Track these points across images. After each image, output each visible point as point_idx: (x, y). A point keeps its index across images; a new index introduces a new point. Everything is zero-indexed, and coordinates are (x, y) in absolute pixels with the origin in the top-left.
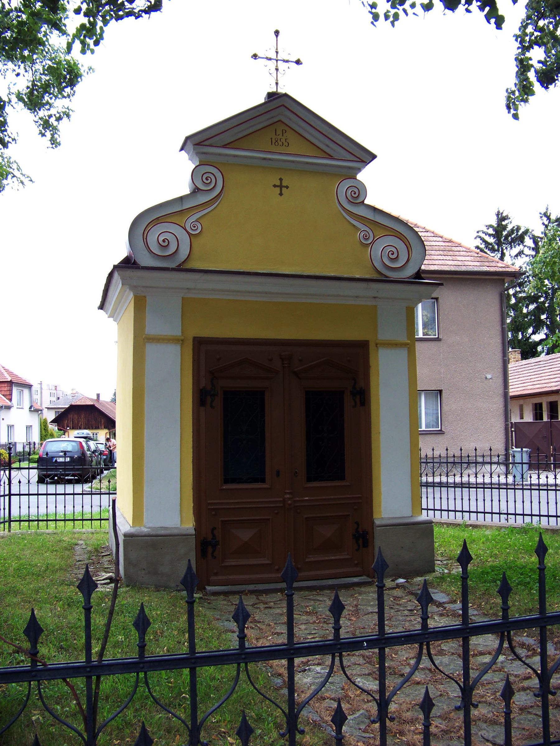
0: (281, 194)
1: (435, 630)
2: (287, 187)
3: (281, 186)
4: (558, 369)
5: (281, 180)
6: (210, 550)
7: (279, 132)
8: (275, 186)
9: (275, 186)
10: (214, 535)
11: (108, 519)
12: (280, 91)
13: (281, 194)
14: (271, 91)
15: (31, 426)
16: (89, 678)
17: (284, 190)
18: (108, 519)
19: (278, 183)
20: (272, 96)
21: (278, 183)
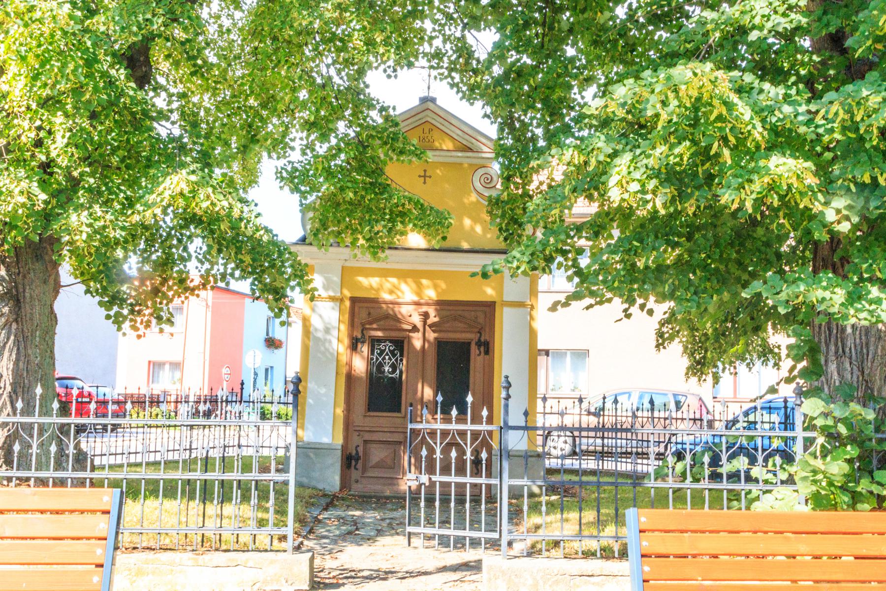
0: (425, 183)
1: (609, 465)
2: (430, 177)
3: (425, 176)
4: (12, 525)
5: (425, 171)
6: (353, 463)
7: (426, 130)
8: (420, 176)
9: (420, 176)
10: (357, 451)
11: (108, 512)
12: (431, 95)
13: (425, 183)
14: (422, 96)
15: (272, 367)
16: (603, 426)
17: (427, 179)
18: (108, 512)
19: (423, 174)
20: (424, 100)
21: (423, 174)
